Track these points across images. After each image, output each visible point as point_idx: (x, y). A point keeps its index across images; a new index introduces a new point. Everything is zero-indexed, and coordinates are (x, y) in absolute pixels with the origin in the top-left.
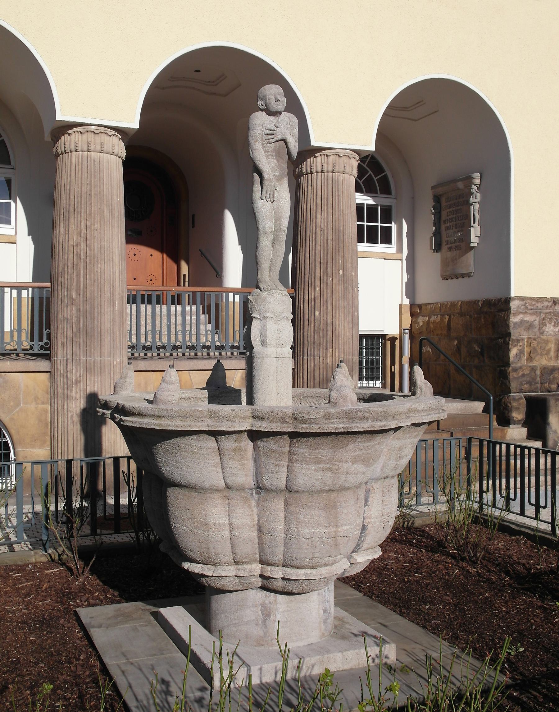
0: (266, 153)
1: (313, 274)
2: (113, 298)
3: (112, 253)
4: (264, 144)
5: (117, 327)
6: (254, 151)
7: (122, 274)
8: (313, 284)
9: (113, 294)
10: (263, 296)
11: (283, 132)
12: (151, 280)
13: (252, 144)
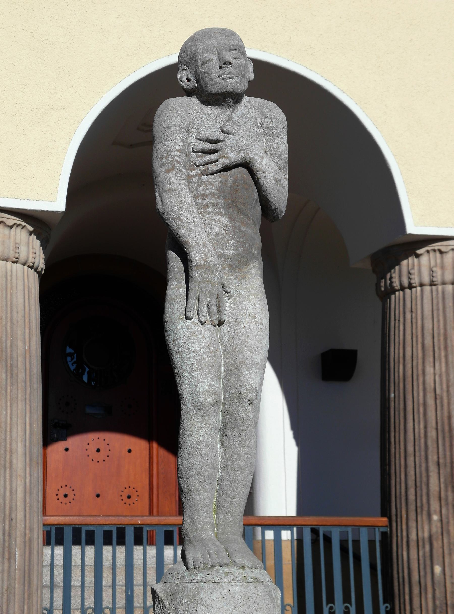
0: (199, 201)
1: (424, 487)
2: (9, 545)
3: (11, 451)
4: (194, 176)
5: (16, 606)
6: (165, 195)
7: (30, 494)
8: (425, 508)
9: (9, 535)
10: (190, 586)
11: (242, 144)
12: (129, 497)
13: (160, 179)
